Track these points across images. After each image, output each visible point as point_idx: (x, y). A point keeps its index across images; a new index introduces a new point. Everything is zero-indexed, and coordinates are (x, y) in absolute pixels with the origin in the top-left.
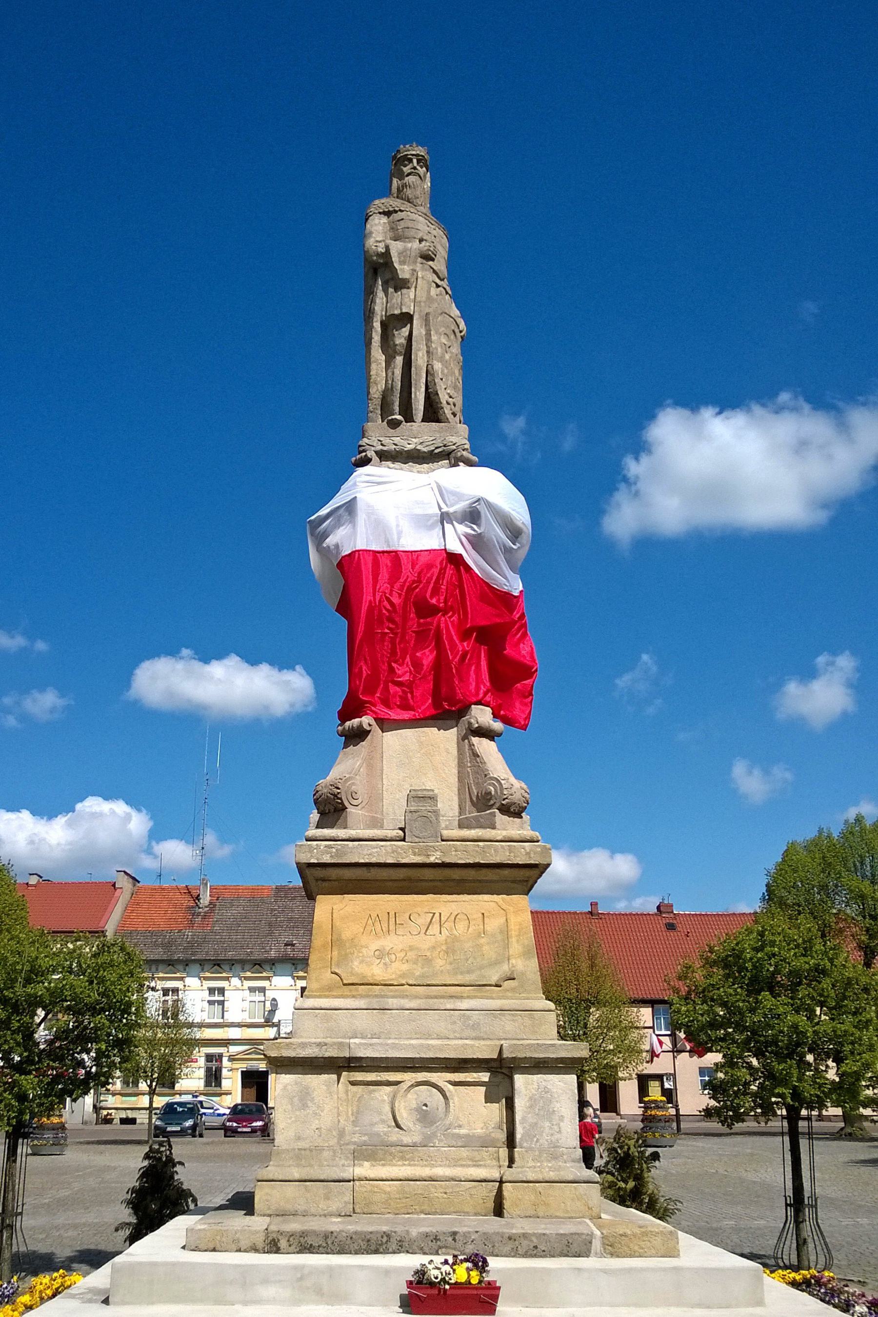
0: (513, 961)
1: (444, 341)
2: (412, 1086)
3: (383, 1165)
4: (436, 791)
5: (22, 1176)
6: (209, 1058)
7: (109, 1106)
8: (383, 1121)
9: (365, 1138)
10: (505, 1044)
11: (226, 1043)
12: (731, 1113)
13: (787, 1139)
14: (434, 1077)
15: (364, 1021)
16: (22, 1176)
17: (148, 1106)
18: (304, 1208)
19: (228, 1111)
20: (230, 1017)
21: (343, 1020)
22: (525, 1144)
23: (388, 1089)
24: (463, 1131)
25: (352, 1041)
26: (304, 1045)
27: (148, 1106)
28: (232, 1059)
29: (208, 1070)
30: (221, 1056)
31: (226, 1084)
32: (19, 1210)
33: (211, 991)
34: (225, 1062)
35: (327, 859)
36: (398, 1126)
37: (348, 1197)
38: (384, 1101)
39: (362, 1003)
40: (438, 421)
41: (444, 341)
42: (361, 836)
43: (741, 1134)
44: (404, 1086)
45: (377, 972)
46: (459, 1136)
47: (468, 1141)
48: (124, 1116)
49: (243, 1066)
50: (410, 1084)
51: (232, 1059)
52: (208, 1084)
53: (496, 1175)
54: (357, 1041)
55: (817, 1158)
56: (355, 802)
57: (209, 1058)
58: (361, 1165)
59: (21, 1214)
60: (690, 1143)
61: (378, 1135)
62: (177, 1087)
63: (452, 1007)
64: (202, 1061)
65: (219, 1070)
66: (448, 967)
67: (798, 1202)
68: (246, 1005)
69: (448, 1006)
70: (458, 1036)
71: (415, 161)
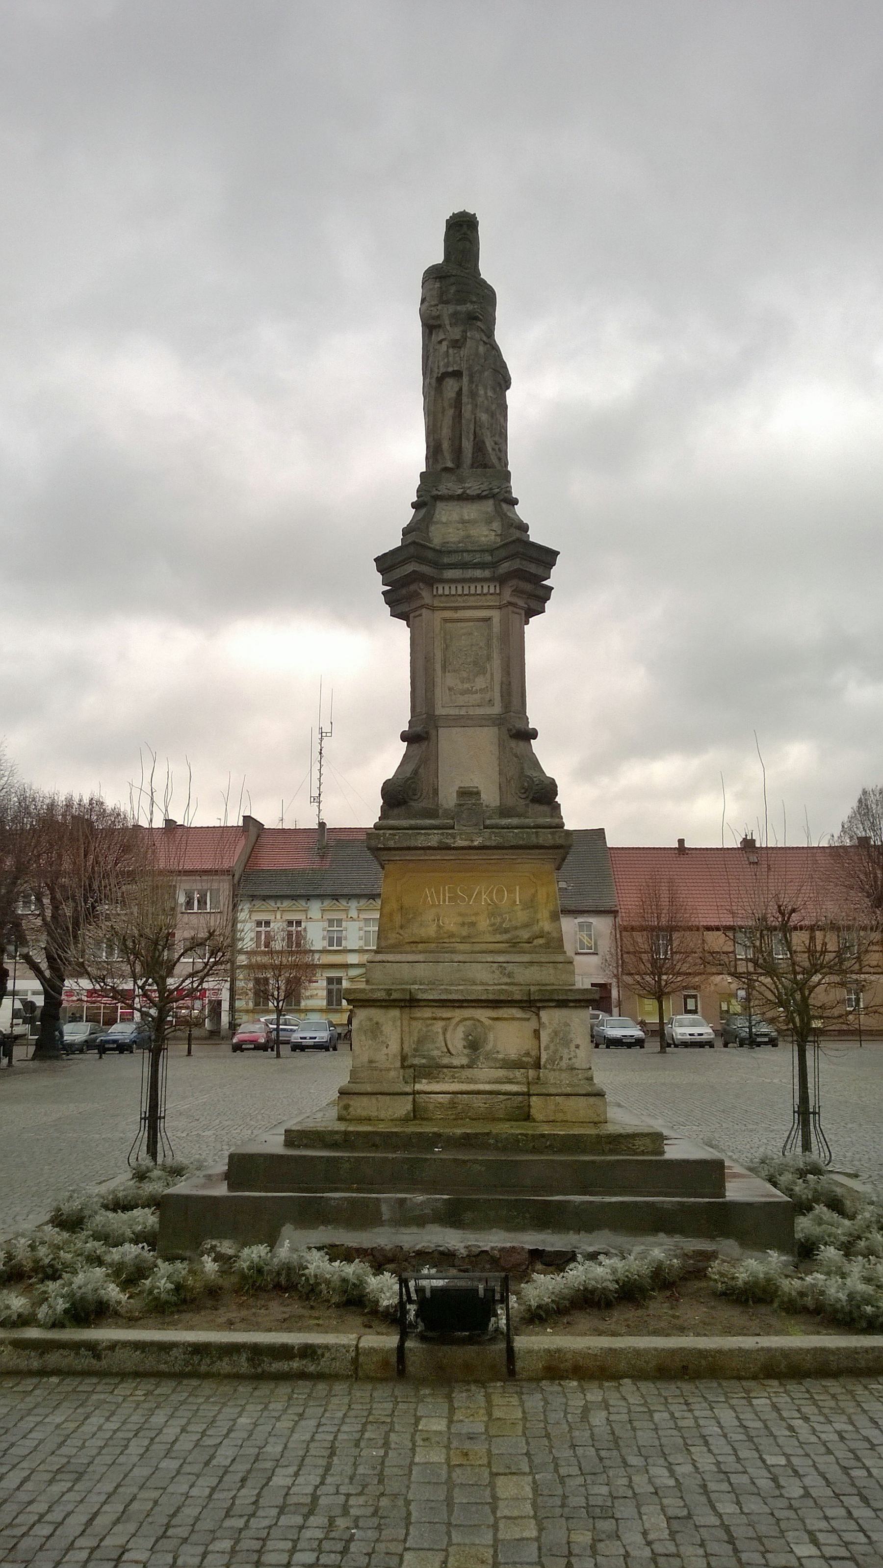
0: (541, 923)
2: (461, 1021)
3: (438, 1082)
4: (480, 788)
5: (164, 1089)
6: (330, 980)
8: (438, 1048)
9: (424, 1061)
10: (533, 988)
11: (346, 966)
16: (164, 1089)
18: (376, 1114)
20: (348, 944)
22: (548, 1066)
24: (500, 1056)
25: (412, 987)
29: (330, 992)
32: (162, 1115)
33: (331, 922)
37: (409, 1107)
39: (420, 957)
43: (389, 1094)
44: (454, 1021)
46: (496, 1059)
50: (458, 1019)
52: (330, 1002)
54: (416, 987)
57: (330, 980)
58: (420, 1082)
59: (164, 1118)
60: (759, 1056)
61: (433, 1058)
62: (303, 1004)
63: (492, 960)
66: (490, 928)
67: (805, 1113)
68: (362, 933)
69: (489, 960)
70: (496, 982)
71: (465, 226)
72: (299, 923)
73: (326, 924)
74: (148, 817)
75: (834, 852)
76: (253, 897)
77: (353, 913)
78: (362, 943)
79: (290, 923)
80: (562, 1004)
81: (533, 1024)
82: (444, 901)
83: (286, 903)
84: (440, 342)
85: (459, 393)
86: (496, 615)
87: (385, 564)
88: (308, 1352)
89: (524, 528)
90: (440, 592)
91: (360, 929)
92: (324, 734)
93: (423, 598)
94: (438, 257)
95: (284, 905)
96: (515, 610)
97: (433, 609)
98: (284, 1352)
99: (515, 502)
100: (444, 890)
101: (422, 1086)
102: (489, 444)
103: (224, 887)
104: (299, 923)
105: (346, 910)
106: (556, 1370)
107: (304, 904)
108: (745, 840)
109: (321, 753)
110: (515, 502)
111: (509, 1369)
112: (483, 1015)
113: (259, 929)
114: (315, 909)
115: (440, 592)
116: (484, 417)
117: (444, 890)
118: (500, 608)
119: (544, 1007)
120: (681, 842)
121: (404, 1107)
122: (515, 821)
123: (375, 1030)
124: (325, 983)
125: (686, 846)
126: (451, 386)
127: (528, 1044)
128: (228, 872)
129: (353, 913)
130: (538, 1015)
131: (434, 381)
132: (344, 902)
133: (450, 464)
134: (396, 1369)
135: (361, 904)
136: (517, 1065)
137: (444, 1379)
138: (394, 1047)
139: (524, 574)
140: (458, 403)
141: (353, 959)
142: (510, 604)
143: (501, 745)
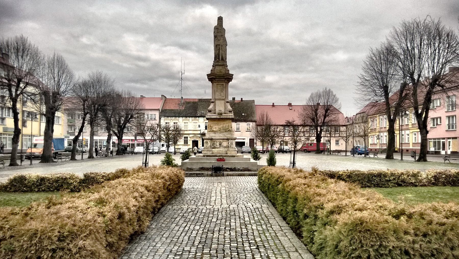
6: (185, 138)
11: (189, 134)
12: (243, 114)
13: (397, 145)
15: (213, 135)
19: (369, 135)
21: (211, 135)
28: (190, 138)
29: (185, 140)
31: (189, 143)
34: (189, 138)
45: (215, 130)
47: (224, 147)
49: (193, 139)
51: (190, 138)
52: (185, 143)
55: (146, 108)
57: (185, 138)
62: (178, 143)
64: (183, 138)
65: (187, 140)
76: (165, 116)
79: (174, 123)
80: (232, 139)
83: (173, 118)
86: (224, 84)
87: (208, 75)
88: (202, 174)
94: (216, 24)
98: (200, 174)
101: (213, 150)
102: (224, 57)
103: (157, 114)
106: (228, 175)
108: (289, 104)
111: (223, 175)
112: (221, 141)
116: (223, 52)
120: (273, 103)
121: (211, 152)
123: (207, 143)
127: (227, 144)
128: (158, 110)
132: (188, 118)
134: (211, 175)
136: (226, 147)
137: (216, 176)
138: (209, 145)
140: (219, 49)
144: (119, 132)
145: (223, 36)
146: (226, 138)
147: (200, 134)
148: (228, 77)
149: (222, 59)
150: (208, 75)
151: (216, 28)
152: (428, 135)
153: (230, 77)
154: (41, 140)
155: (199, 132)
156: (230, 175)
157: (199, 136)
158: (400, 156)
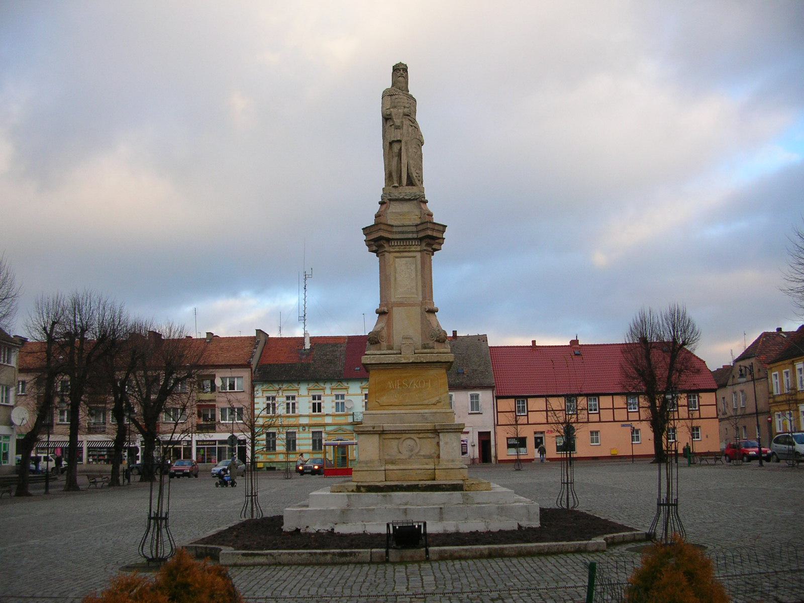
1: (414, 150)
2: (405, 439)
7: (309, 454)
11: (324, 425)
14: (412, 436)
17: (612, 407)
23: (397, 441)
26: (366, 427)
27: (612, 407)
28: (328, 433)
30: (321, 432)
33: (337, 396)
35: (373, 362)
36: (400, 452)
38: (410, 360)
40: (414, 186)
41: (414, 150)
42: (385, 353)
48: (269, 466)
51: (328, 433)
52: (314, 448)
53: (433, 468)
56: (383, 340)
68: (334, 404)
71: (402, 71)
72: (293, 398)
73: (334, 398)
74: (199, 333)
75: (625, 348)
77: (328, 391)
78: (334, 410)
81: (436, 440)
82: (397, 387)
84: (391, 126)
85: (400, 149)
87: (367, 231)
89: (431, 215)
90: (393, 244)
91: (333, 401)
92: (307, 276)
93: (385, 247)
95: (283, 387)
96: (427, 253)
97: (390, 252)
99: (426, 202)
100: (397, 382)
102: (414, 175)
103: (246, 374)
104: (293, 398)
105: (323, 389)
106: (442, 558)
107: (297, 386)
109: (305, 288)
110: (426, 202)
113: (288, 401)
114: (303, 389)
115: (393, 244)
117: (397, 382)
118: (420, 251)
119: (441, 432)
122: (428, 351)
124: (311, 435)
125: (536, 345)
126: (396, 147)
129: (328, 391)
130: (439, 436)
131: (388, 144)
133: (396, 185)
134: (385, 561)
135: (333, 385)
139: (430, 237)
140: (399, 155)
141: (328, 420)
142: (425, 250)
143: (422, 313)
144: (147, 426)
145: (410, 115)
146: (429, 426)
147: (351, 424)
148: (430, 233)
149: (410, 183)
150: (367, 231)
151: (387, 94)
152: (240, 477)
153: (435, 234)
154: (680, 460)
155: (350, 419)
156: (453, 557)
157: (349, 428)
158: (279, 455)
